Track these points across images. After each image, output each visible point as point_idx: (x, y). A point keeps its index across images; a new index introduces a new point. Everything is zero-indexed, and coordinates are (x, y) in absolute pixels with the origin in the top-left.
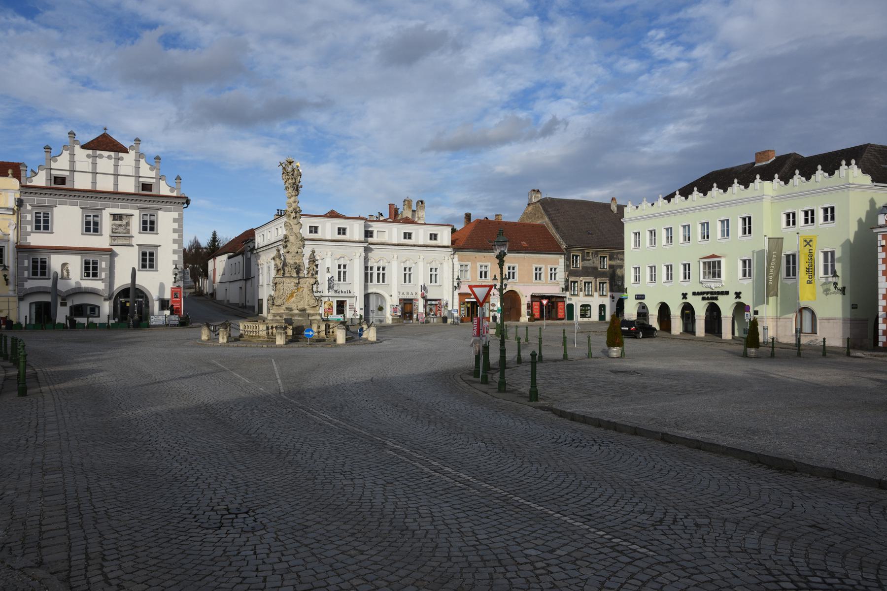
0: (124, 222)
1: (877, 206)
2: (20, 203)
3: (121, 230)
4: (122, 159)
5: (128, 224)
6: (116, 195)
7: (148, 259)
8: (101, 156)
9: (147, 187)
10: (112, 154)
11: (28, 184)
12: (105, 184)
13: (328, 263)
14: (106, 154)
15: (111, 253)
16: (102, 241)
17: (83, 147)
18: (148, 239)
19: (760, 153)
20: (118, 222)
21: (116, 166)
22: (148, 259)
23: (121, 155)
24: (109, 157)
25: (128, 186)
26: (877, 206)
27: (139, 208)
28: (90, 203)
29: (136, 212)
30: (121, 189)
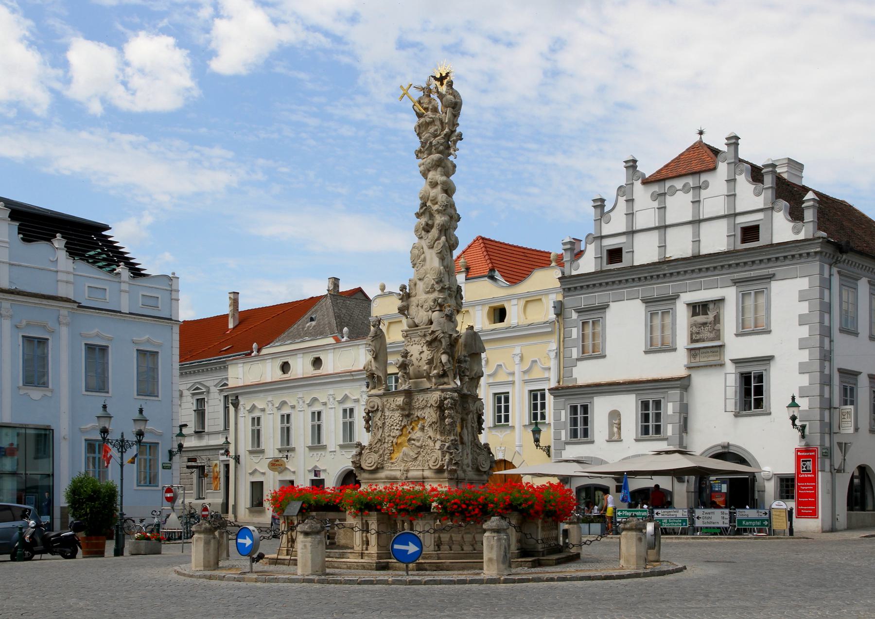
0: (711, 316)
1: (342, 289)
2: (560, 310)
3: (706, 333)
4: (706, 185)
5: (717, 319)
6: (699, 265)
7: (752, 392)
8: (673, 191)
9: (750, 233)
10: (690, 181)
11: (574, 273)
12: (680, 245)
14: (679, 184)
15: (683, 384)
16: (672, 365)
17: (646, 182)
19: (489, 449)
20: (701, 319)
21: (696, 202)
22: (752, 392)
23: (704, 177)
24: (686, 189)
25: (717, 239)
26: (342, 289)
27: (736, 282)
28: (656, 290)
29: (730, 294)
30: (706, 249)
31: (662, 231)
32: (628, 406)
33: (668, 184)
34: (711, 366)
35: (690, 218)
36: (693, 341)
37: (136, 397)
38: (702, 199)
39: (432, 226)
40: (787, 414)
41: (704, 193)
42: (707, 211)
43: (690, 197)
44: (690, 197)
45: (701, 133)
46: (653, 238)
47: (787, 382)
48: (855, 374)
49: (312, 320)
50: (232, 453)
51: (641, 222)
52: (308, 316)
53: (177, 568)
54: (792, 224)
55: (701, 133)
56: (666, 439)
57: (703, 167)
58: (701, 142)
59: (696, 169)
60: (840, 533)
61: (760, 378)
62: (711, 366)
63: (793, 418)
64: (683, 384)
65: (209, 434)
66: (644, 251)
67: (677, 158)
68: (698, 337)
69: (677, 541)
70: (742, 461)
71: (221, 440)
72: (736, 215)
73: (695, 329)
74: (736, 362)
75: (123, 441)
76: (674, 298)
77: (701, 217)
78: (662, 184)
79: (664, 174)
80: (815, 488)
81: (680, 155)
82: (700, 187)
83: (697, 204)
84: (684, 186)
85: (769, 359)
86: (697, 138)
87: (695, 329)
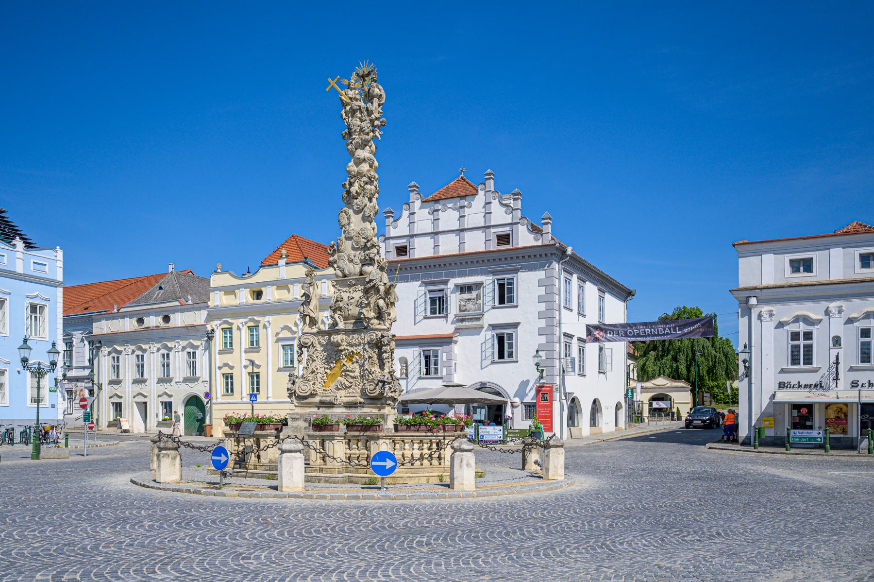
7: (503, 347)
9: (503, 239)
12: (449, 246)
13: (837, 327)
18: (503, 316)
20: (466, 296)
25: (475, 243)
30: (468, 249)
32: (412, 354)
34: (844, 283)
36: (460, 311)
40: (532, 362)
42: (468, 223)
46: (428, 241)
47: (526, 342)
48: (571, 337)
49: (161, 288)
50: (96, 382)
51: (419, 228)
52: (157, 285)
53: (135, 476)
54: (533, 236)
56: (441, 378)
57: (467, 193)
59: (463, 194)
61: (510, 336)
62: (844, 283)
63: (537, 365)
64: (446, 340)
65: (601, 299)
66: (422, 249)
68: (465, 308)
69: (850, 459)
70: (498, 394)
71: (86, 372)
72: (489, 227)
73: (462, 303)
74: (494, 327)
75: (39, 369)
76: (446, 282)
77: (466, 227)
80: (551, 412)
85: (516, 325)
87: (462, 303)
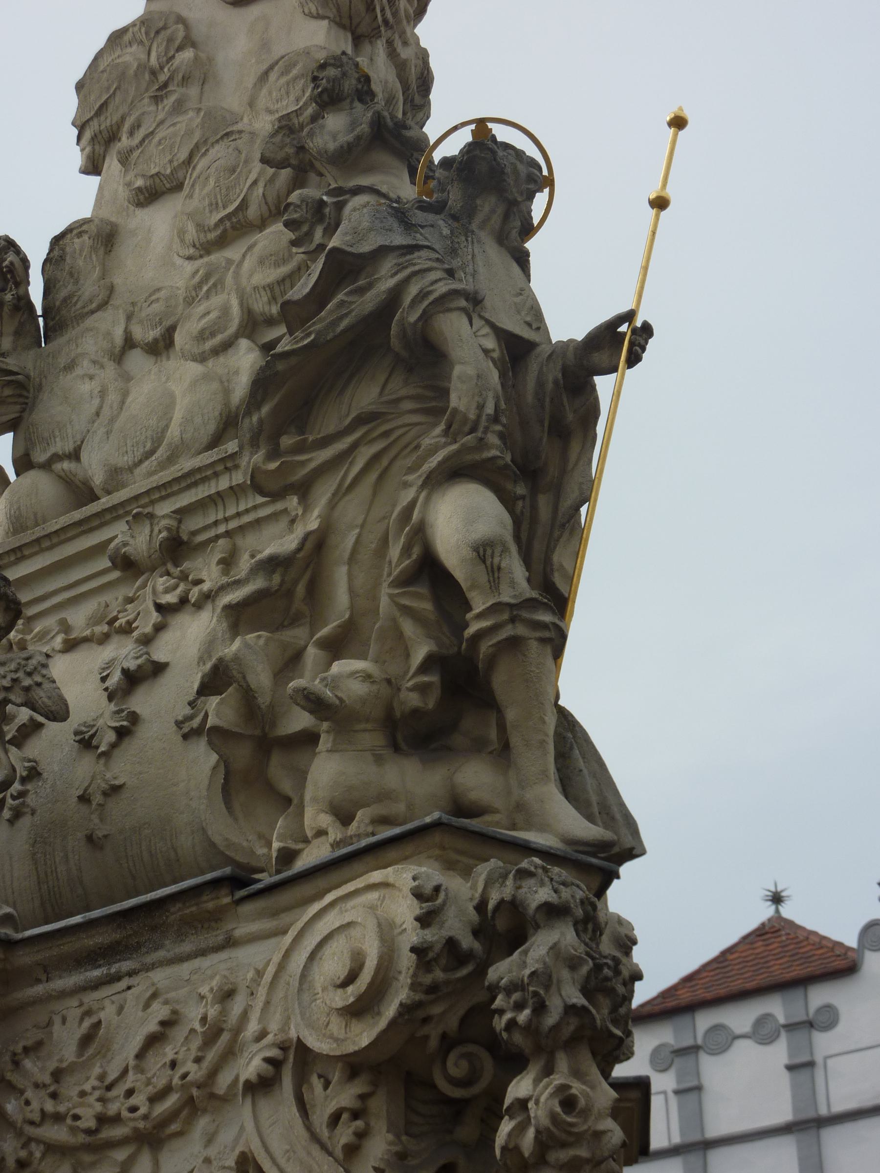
4: (828, 1019)
8: (721, 1041)
10: (775, 1007)
14: (740, 1018)
21: (801, 1067)
23: (819, 996)
24: (763, 1033)
31: (694, 1158)
33: (704, 1021)
35: (784, 1114)
37: (242, 1079)
38: (819, 1059)
39: (542, 880)
41: (824, 1043)
43: (779, 1053)
44: (779, 1053)
45: (777, 899)
55: (777, 899)
58: (778, 917)
60: (104, 405)
67: (715, 960)
77: (823, 1111)
78: (683, 1021)
79: (685, 996)
81: (724, 953)
82: (810, 1025)
83: (804, 1074)
84: (760, 1022)
86: (766, 912)
